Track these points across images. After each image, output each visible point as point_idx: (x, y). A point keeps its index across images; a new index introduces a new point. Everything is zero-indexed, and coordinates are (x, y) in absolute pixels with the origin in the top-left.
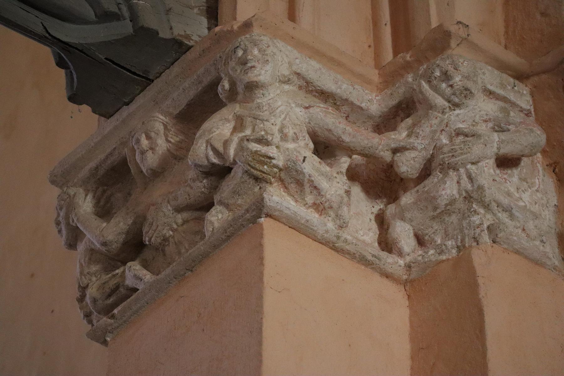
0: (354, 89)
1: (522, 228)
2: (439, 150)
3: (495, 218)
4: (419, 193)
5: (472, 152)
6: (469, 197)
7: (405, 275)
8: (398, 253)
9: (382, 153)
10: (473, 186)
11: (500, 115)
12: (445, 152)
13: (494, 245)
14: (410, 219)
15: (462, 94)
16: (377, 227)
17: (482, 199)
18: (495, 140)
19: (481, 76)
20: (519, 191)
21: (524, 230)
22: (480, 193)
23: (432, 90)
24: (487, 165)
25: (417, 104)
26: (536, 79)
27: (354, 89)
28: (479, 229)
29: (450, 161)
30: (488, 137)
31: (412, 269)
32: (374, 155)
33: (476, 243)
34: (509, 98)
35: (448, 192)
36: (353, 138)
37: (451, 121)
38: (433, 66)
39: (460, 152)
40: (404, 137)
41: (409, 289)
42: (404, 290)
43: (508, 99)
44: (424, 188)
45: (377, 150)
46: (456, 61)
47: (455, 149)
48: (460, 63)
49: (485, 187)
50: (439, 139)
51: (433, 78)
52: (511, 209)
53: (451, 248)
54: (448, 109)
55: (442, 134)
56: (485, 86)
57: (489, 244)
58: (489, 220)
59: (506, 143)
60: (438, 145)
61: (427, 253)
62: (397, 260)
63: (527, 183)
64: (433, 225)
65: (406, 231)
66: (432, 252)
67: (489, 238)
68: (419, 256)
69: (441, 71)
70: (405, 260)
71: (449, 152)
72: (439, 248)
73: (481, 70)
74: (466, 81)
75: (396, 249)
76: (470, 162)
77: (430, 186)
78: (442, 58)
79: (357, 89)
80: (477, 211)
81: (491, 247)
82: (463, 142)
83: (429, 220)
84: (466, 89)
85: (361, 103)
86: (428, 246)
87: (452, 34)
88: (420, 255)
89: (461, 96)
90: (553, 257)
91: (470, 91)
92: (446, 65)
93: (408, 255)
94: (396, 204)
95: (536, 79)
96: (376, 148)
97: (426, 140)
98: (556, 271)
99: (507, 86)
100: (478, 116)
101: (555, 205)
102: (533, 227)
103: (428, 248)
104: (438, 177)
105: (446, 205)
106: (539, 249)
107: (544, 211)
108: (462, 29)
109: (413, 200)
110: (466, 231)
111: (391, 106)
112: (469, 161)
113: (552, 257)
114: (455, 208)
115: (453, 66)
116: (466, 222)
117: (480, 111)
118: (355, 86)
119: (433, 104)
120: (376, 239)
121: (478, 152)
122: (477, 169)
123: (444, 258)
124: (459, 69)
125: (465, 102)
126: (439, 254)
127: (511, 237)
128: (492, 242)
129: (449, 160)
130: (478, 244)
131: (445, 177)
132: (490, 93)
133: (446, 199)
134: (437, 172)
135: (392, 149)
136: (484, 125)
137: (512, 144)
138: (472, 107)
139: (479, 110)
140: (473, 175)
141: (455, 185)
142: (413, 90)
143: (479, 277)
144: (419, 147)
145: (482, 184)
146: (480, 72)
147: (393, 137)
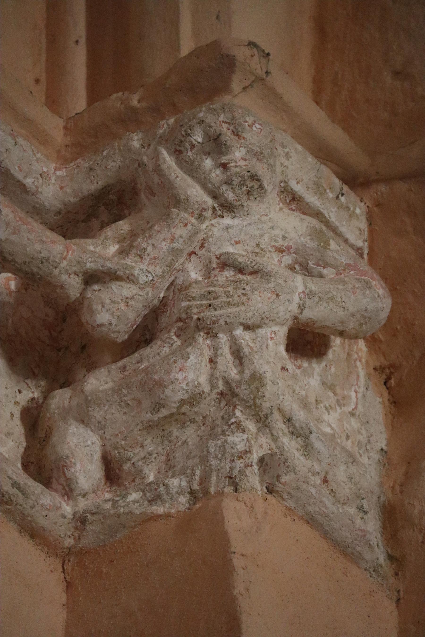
0: (16, 145)
1: (323, 477)
2: (180, 291)
3: (274, 446)
4: (127, 373)
5: (250, 303)
6: (229, 393)
7: (70, 537)
8: (64, 488)
9: (64, 277)
10: (241, 372)
11: (310, 244)
12: (193, 295)
13: (269, 497)
14: (99, 422)
15: (243, 185)
16: (23, 431)
17: (257, 401)
18: (296, 288)
19: (283, 160)
20: (319, 407)
21: (325, 481)
22: (254, 389)
23: (181, 169)
24: (273, 336)
25: (143, 196)
26: (383, 189)
27: (16, 145)
28: (242, 460)
29: (202, 314)
30: (285, 281)
31: (88, 527)
32: (49, 278)
33: (232, 488)
34: (327, 215)
35: (191, 376)
36: (14, 233)
37: (211, 236)
38: (190, 120)
39: (225, 299)
40: (111, 253)
41: (73, 569)
42: (61, 570)
43: (325, 217)
44: (138, 362)
45: (56, 268)
46: (239, 119)
47: (215, 292)
48: (247, 124)
49: (266, 378)
50: (183, 270)
51: (188, 145)
52: (307, 433)
53: (177, 492)
54: (210, 212)
55: (190, 261)
56: (285, 182)
57: (259, 493)
58: (262, 448)
59: (316, 299)
60: (179, 281)
61: (123, 497)
62: (60, 503)
63: (335, 394)
64: (146, 443)
65: (88, 446)
66: (134, 496)
67: (261, 481)
68: (106, 501)
69: (206, 134)
70: (77, 506)
71: (203, 297)
72: (151, 490)
73: (284, 147)
74: (254, 160)
75: (62, 480)
76: (242, 324)
77: (151, 361)
78: (210, 109)
79: (21, 146)
80: (243, 423)
81: (262, 501)
82: (233, 281)
83: (140, 430)
84: (254, 178)
85: (25, 177)
86: (125, 485)
87: (237, 64)
88: (109, 500)
89: (241, 189)
90: (378, 545)
91: (259, 184)
92: (218, 122)
93: (84, 496)
94: (73, 390)
95: (383, 188)
96: (56, 264)
97: (158, 267)
98: (379, 576)
99: (328, 191)
100: (266, 237)
101: (382, 450)
102: (345, 479)
103: (127, 488)
104: (172, 345)
105: (183, 402)
106: (353, 523)
107: (361, 456)
108: (256, 58)
109: (110, 384)
110: (214, 462)
111: (86, 193)
112: (241, 320)
113: (375, 544)
114: (196, 413)
115: (231, 128)
116: (216, 445)
117: (272, 228)
118: (18, 140)
119: (183, 197)
120: (19, 456)
121: (260, 305)
122: (254, 341)
123: (160, 510)
124: (244, 135)
125: (245, 205)
126: (149, 501)
127: (305, 486)
128: (266, 491)
129: (200, 313)
130: (236, 490)
131: (187, 347)
132: (293, 199)
133: (183, 389)
134: (172, 334)
135: (85, 273)
136: (276, 257)
137: (328, 303)
138: (258, 216)
139: (271, 225)
140: (246, 350)
141: (206, 366)
142: (139, 165)
143: (236, 555)
144: (142, 279)
145: (261, 372)
146: (282, 153)
147: (92, 248)
